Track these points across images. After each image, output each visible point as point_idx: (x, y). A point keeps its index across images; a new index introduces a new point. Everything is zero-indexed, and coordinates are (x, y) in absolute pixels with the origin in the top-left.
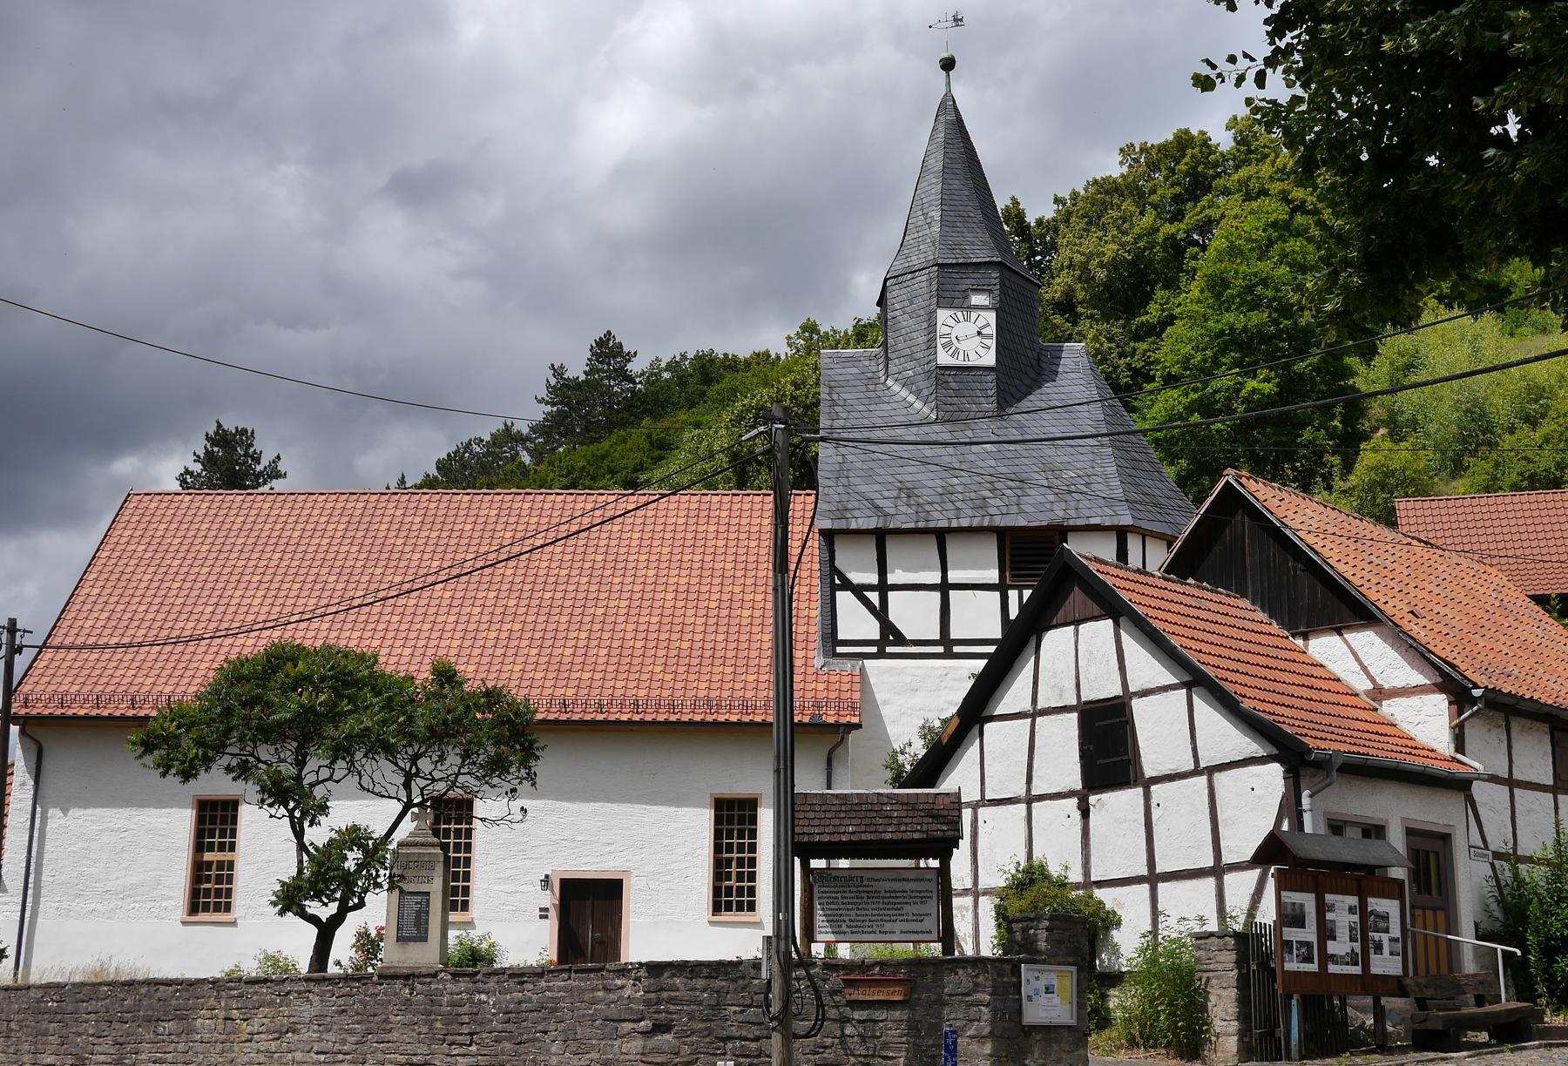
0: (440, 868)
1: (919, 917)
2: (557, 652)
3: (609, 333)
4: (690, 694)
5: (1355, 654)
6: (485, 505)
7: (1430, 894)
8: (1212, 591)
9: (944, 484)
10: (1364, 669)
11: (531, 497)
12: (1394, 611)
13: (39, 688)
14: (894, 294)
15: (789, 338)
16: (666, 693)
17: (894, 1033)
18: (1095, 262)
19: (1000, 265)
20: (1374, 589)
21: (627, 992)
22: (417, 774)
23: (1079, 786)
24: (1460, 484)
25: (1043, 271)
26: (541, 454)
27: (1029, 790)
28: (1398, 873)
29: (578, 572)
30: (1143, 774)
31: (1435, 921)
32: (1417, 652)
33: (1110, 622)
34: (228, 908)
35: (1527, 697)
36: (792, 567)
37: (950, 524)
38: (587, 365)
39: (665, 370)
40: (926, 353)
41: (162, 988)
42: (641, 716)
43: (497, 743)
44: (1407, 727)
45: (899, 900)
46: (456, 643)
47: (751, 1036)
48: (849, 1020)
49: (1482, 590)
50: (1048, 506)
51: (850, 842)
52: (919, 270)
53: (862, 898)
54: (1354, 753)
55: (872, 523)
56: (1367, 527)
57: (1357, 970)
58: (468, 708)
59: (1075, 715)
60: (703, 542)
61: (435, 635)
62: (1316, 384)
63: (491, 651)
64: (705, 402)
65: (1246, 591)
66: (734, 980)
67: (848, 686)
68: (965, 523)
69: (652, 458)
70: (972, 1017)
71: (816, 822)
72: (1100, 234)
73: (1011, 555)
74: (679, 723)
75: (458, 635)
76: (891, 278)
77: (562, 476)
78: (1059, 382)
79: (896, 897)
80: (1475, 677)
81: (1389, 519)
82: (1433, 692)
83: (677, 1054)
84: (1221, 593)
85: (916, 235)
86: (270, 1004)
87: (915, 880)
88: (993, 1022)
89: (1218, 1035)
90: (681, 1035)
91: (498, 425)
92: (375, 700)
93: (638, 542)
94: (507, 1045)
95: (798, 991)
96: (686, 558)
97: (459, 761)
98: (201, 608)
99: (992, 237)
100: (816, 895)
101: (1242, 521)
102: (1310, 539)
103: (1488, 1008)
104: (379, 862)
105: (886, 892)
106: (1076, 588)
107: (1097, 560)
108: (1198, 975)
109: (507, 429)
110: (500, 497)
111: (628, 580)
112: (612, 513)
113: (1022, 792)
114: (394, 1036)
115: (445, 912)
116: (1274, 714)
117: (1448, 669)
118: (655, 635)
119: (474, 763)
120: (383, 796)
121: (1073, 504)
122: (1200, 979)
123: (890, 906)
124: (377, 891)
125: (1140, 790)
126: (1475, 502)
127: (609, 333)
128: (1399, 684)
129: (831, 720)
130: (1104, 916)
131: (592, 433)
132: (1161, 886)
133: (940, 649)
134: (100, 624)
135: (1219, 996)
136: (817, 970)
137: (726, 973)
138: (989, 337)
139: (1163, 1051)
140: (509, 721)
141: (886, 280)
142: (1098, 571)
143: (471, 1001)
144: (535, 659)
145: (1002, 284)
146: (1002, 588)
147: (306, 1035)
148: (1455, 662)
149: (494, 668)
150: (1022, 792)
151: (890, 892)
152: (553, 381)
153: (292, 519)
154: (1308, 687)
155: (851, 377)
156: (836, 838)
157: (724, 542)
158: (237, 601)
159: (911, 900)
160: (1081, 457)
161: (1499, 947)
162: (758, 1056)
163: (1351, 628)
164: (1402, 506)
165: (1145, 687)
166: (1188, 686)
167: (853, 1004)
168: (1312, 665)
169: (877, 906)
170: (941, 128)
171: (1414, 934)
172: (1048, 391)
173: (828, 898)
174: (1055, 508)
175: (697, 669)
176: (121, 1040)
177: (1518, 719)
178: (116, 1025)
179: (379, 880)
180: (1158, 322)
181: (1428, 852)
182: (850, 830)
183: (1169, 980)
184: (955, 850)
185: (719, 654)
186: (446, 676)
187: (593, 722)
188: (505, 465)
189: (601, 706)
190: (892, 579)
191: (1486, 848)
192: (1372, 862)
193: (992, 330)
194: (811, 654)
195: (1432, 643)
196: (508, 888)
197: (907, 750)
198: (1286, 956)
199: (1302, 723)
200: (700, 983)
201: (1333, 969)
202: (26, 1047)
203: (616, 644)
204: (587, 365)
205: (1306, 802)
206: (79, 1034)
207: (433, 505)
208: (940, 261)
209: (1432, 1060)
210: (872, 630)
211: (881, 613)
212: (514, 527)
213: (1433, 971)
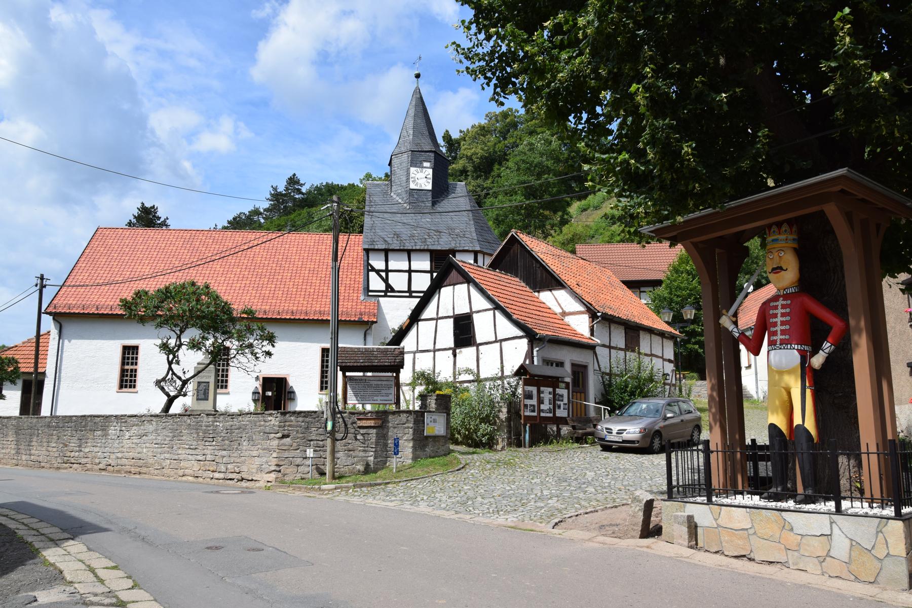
1: (387, 395)
2: (263, 292)
4: (313, 309)
5: (556, 299)
7: (579, 386)
10: (559, 304)
13: (60, 302)
14: (395, 161)
16: (304, 308)
19: (434, 152)
20: (564, 275)
21: (272, 423)
23: (453, 346)
28: (568, 380)
31: (581, 398)
34: (134, 387)
41: (96, 418)
46: (224, 288)
47: (320, 439)
49: (603, 277)
51: (361, 366)
55: (383, 247)
56: (569, 255)
57: (551, 415)
59: (452, 320)
68: (418, 248)
74: (308, 319)
75: (225, 285)
81: (573, 252)
86: (137, 425)
88: (414, 434)
91: (251, 208)
94: (227, 442)
96: (313, 258)
98: (125, 273)
100: (348, 386)
101: (516, 247)
102: (542, 256)
107: (462, 261)
111: (291, 266)
114: (184, 438)
117: (589, 305)
118: (301, 287)
125: (475, 348)
126: (604, 246)
128: (572, 310)
129: (366, 320)
131: (287, 212)
133: (408, 294)
134: (85, 277)
138: (430, 179)
141: (392, 156)
145: (435, 159)
146: (431, 272)
147: (151, 437)
153: (162, 239)
156: (355, 364)
158: (139, 270)
162: (323, 447)
163: (554, 289)
164: (578, 247)
170: (414, 100)
171: (573, 401)
176: (81, 438)
178: (78, 432)
182: (361, 362)
189: (279, 313)
192: (558, 375)
193: (431, 176)
194: (359, 295)
198: (525, 410)
200: (301, 419)
201: (542, 414)
202: (45, 440)
203: (286, 289)
205: (535, 353)
206: (65, 436)
210: (382, 287)
211: (386, 281)
213: (579, 415)
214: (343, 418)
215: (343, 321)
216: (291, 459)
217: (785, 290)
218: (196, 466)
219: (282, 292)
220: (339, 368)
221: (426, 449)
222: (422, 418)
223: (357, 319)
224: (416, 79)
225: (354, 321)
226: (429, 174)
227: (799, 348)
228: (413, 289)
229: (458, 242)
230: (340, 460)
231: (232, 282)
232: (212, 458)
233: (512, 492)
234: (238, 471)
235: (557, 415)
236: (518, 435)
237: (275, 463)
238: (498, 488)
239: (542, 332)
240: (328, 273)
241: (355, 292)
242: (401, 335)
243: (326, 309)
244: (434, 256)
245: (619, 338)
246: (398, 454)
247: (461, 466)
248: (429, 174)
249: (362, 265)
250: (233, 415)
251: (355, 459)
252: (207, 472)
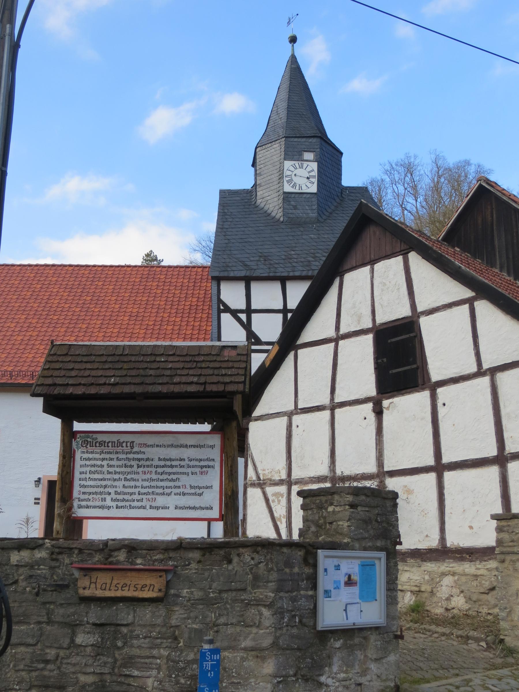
3: (151, 251)
9: (286, 254)
23: (373, 392)
45: (174, 470)
52: (275, 141)
53: (131, 466)
55: (243, 274)
59: (370, 337)
68: (297, 274)
79: (172, 466)
87: (194, 446)
105: (160, 459)
113: (325, 400)
123: (165, 477)
125: (426, 394)
127: (151, 251)
132: (448, 475)
138: (314, 177)
151: (165, 460)
159: (190, 470)
169: (148, 476)
173: (92, 466)
193: (315, 173)
211: (247, 326)
221: (323, 679)
222: (308, 570)
224: (291, 45)
226: (313, 170)
248: (313, 170)
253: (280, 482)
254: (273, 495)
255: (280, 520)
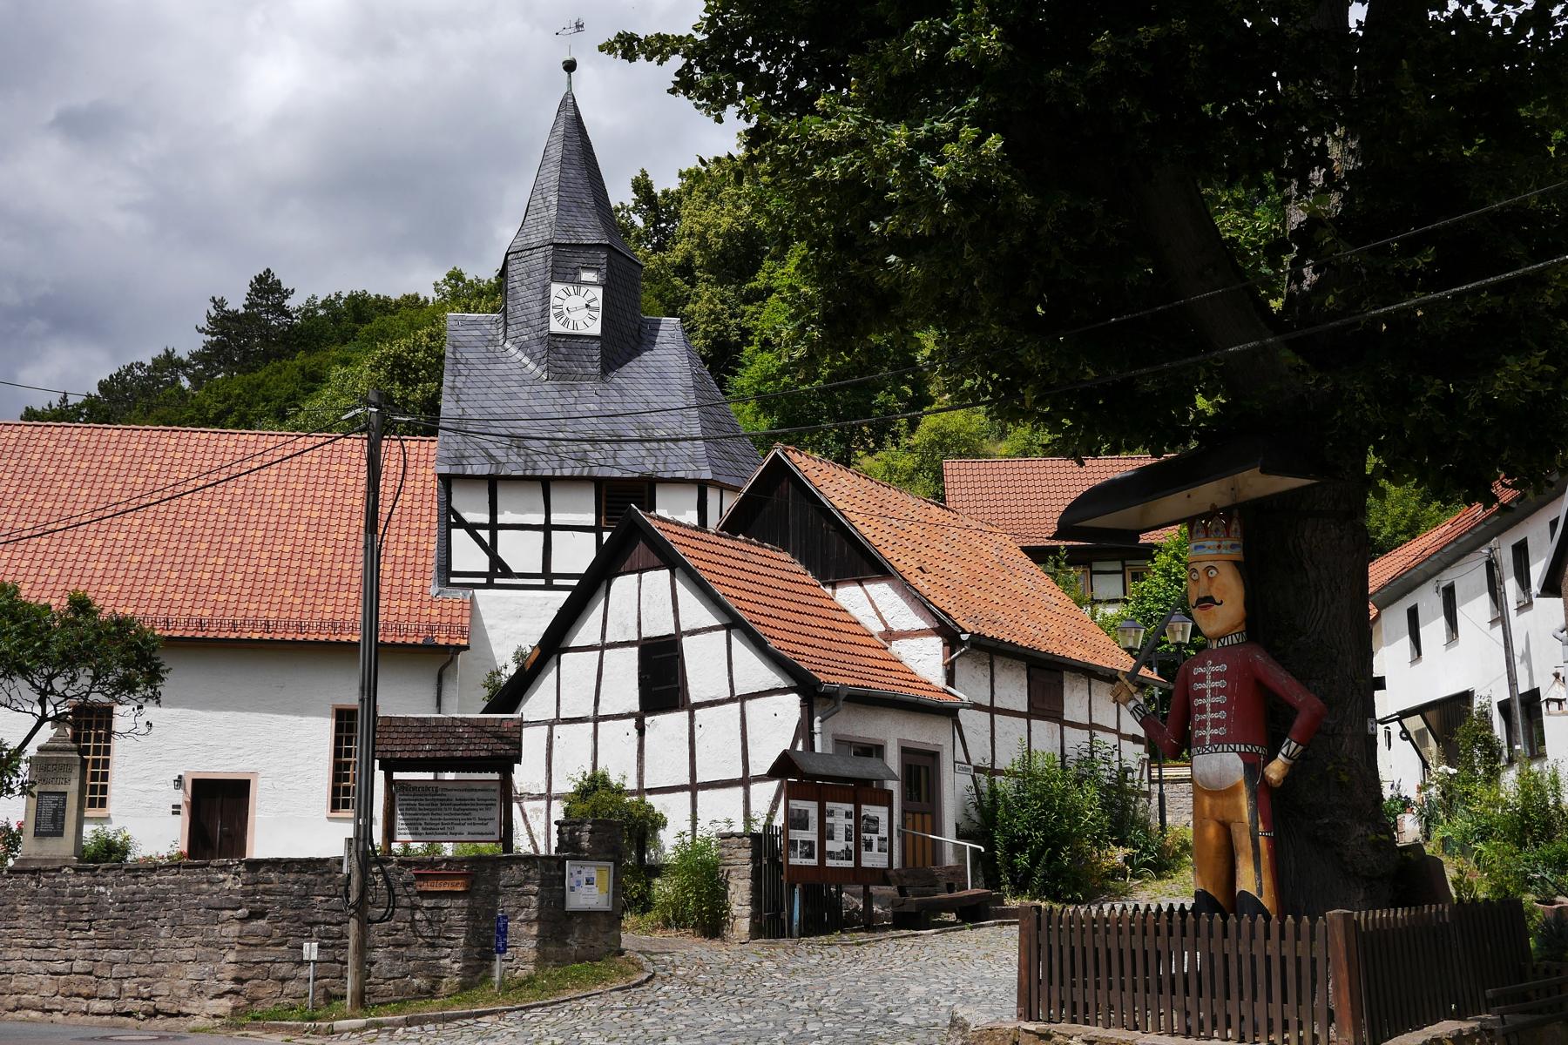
0: (77, 771)
1: (484, 822)
3: (268, 270)
4: (317, 616)
5: (872, 602)
6: (134, 440)
7: (920, 800)
8: (759, 546)
10: (879, 614)
11: (177, 434)
12: (905, 567)
15: (436, 284)
16: (295, 615)
17: (457, 918)
18: (712, 232)
21: (228, 885)
22: (52, 692)
23: (637, 709)
24: (1003, 448)
25: (667, 237)
26: (200, 379)
27: (596, 711)
29: (218, 503)
30: (689, 700)
32: (920, 602)
33: (667, 572)
35: (1007, 640)
36: (381, 531)
37: (554, 472)
38: (247, 299)
39: (321, 308)
40: (540, 321)
42: (271, 635)
43: (126, 665)
44: (910, 664)
47: (334, 921)
48: (418, 908)
49: (985, 549)
50: (640, 460)
54: (858, 686)
57: (850, 864)
58: (99, 635)
59: (636, 649)
60: (334, 481)
61: (82, 557)
62: (889, 354)
63: (134, 574)
64: (355, 340)
65: (788, 544)
66: (321, 875)
67: (459, 612)
68: (567, 472)
69: (304, 389)
70: (522, 904)
71: (398, 742)
72: (718, 207)
73: (607, 502)
74: (305, 642)
76: (512, 253)
77: (219, 402)
78: (656, 351)
80: (964, 625)
82: (932, 635)
83: (269, 937)
84: (766, 548)
85: (536, 216)
88: (540, 908)
89: (734, 918)
90: (273, 921)
92: (13, 627)
93: (275, 478)
94: (121, 930)
95: (376, 883)
97: (89, 682)
99: (602, 221)
100: (397, 802)
102: (841, 505)
103: (956, 894)
104: (12, 770)
106: (641, 542)
108: (721, 868)
109: (169, 355)
110: (148, 433)
112: (237, 470)
113: (590, 713)
114: (21, 922)
115: (81, 809)
116: (796, 652)
117: (943, 617)
118: (287, 563)
119: (104, 684)
120: (19, 711)
121: (662, 459)
122: (723, 872)
124: (9, 796)
125: (686, 714)
127: (268, 270)
129: (442, 642)
130: (653, 818)
131: (248, 363)
132: (700, 794)
133: (542, 582)
135: (737, 885)
136: (393, 865)
137: (315, 869)
138: (596, 309)
139: (691, 931)
140: (137, 647)
141: (507, 254)
142: (659, 528)
143: (91, 892)
144: (233, 525)
145: (609, 263)
146: (597, 529)
148: (950, 611)
149: (137, 589)
150: (590, 713)
152: (213, 313)
154: (830, 629)
155: (473, 339)
156: (414, 755)
157: (354, 481)
160: (671, 418)
161: (968, 845)
162: (340, 938)
163: (870, 580)
165: (693, 627)
166: (728, 627)
167: (424, 895)
168: (837, 610)
170: (561, 122)
172: (659, 352)
174: (646, 461)
175: (324, 594)
177: (1000, 658)
179: (11, 786)
180: (765, 289)
181: (919, 767)
182: (427, 748)
183: (697, 872)
184: (516, 765)
185: (344, 581)
186: (81, 605)
187: (227, 640)
188: (164, 388)
190: (501, 519)
191: (969, 763)
192: (866, 776)
193: (599, 303)
194: (427, 583)
195: (933, 595)
196: (142, 787)
197: (503, 672)
198: (791, 852)
199: (818, 661)
200: (292, 877)
201: (830, 863)
203: (251, 570)
204: (247, 299)
205: (817, 726)
207: (84, 438)
208: (555, 241)
209: (905, 937)
210: (482, 563)
211: (491, 549)
212: (160, 461)
213: (919, 864)
214: (383, 872)
215: (388, 644)
216: (269, 965)
217: (1219, 640)
218: (49, 986)
219: (241, 576)
220: (377, 762)
221: (568, 941)
222: (560, 873)
223: (420, 641)
225: (415, 645)
226: (595, 299)
227: (1243, 750)
228: (554, 570)
229: (662, 459)
230: (376, 966)
231: (120, 551)
232: (88, 965)
233: (744, 1027)
234: (145, 996)
235: (864, 864)
236: (776, 907)
237: (233, 974)
238: (715, 1019)
239: (832, 679)
240: (353, 530)
241: (418, 575)
242: (510, 694)
243: (349, 617)
244: (604, 492)
245: (1013, 691)
246: (505, 952)
247: (645, 976)
248: (595, 299)
249: (435, 512)
250: (137, 870)
251: (411, 964)
252: (73, 999)
253: (540, 797)
254: (531, 810)
255: (538, 837)
